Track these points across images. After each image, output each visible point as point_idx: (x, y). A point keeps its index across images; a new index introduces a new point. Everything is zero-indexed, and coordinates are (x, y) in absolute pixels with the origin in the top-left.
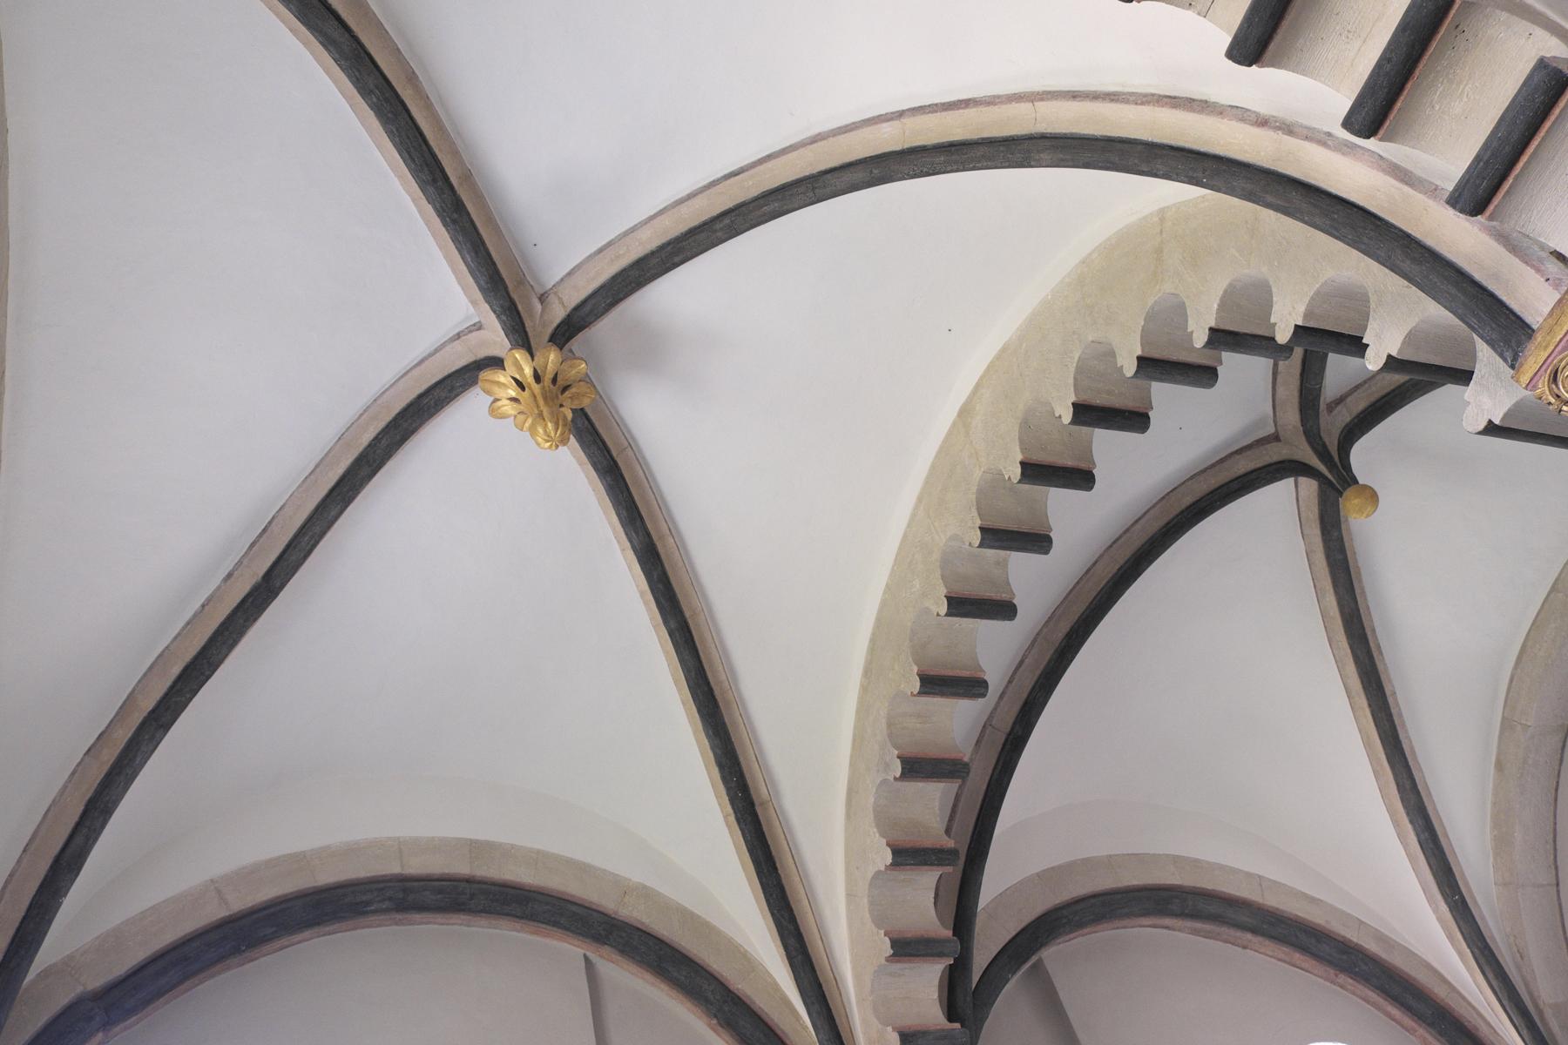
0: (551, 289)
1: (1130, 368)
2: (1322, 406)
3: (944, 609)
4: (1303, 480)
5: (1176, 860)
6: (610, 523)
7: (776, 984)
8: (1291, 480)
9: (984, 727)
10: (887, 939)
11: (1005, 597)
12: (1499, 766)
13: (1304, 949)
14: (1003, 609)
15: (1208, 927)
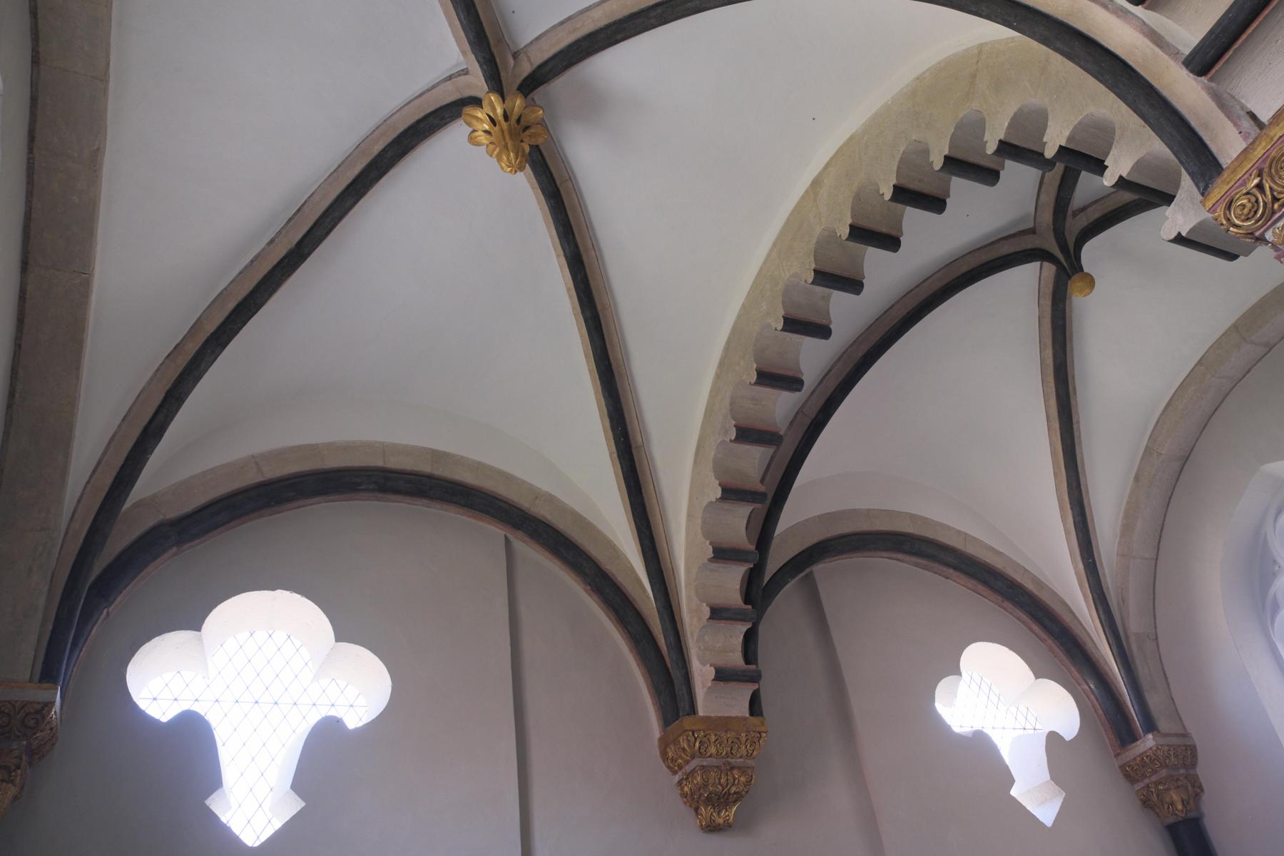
0: (523, 48)
1: (938, 163)
2: (1070, 212)
3: (780, 326)
4: (1046, 264)
5: (913, 517)
6: (551, 236)
7: (633, 568)
8: (1038, 264)
9: (797, 413)
10: (711, 547)
11: (824, 322)
12: (1137, 478)
13: (985, 583)
14: (822, 331)
15: (924, 562)
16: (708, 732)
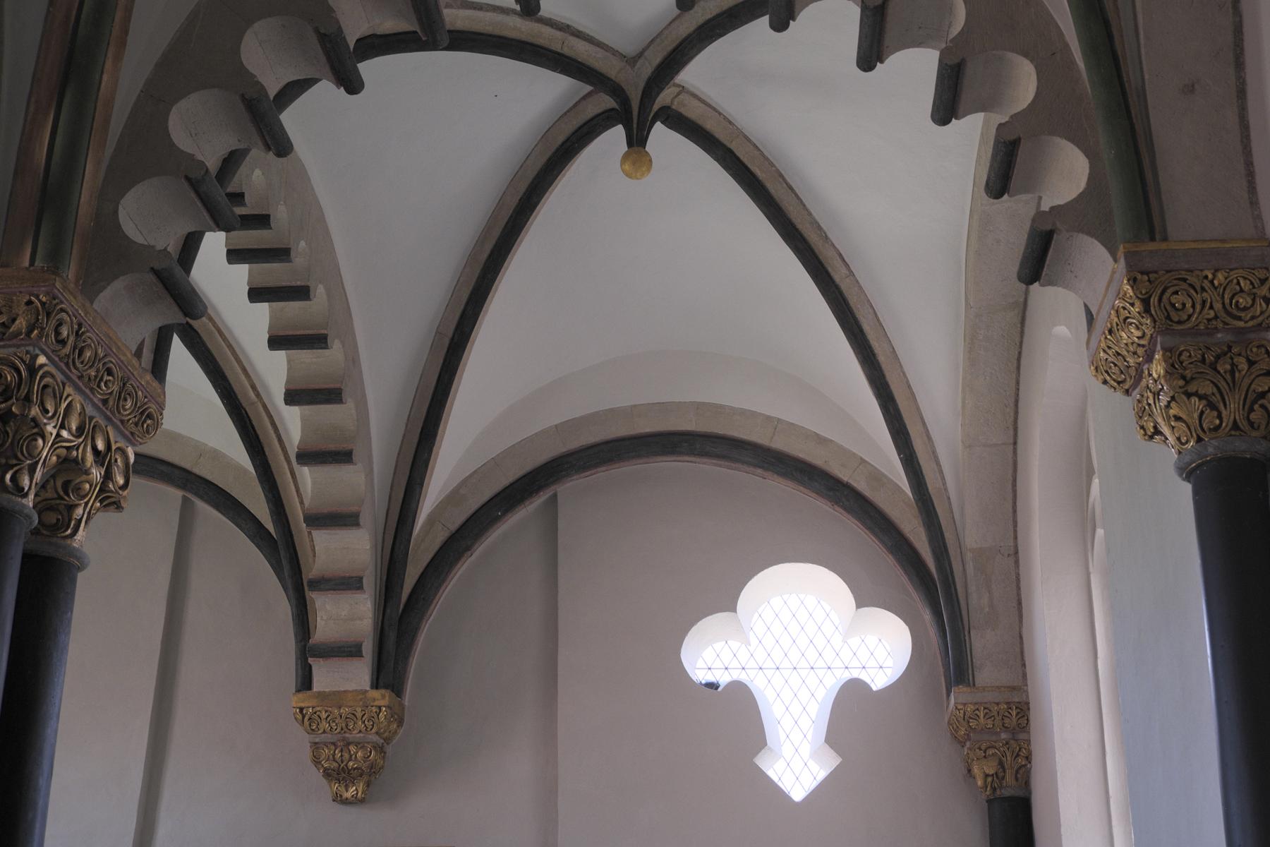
16: (318, 709)
